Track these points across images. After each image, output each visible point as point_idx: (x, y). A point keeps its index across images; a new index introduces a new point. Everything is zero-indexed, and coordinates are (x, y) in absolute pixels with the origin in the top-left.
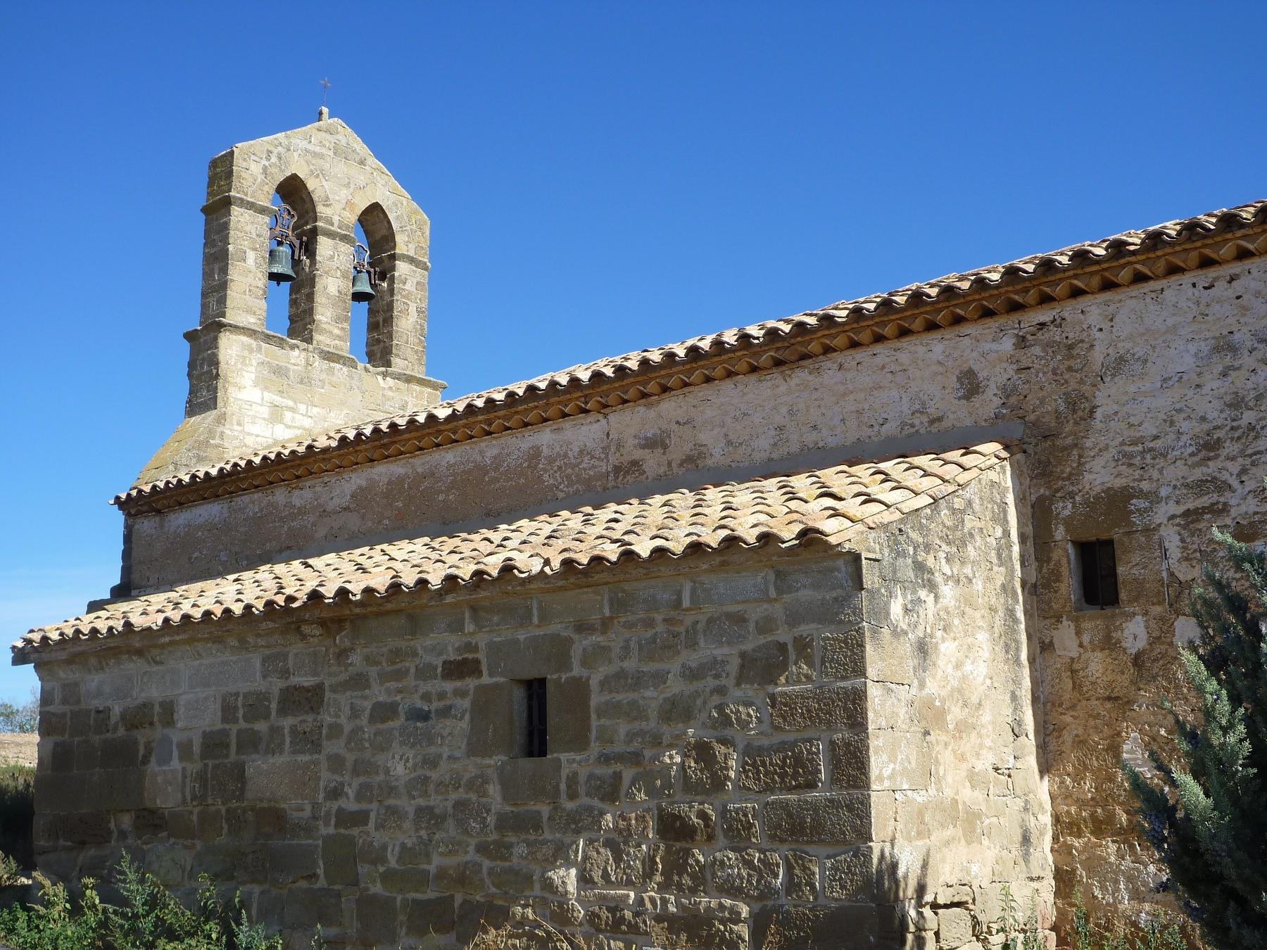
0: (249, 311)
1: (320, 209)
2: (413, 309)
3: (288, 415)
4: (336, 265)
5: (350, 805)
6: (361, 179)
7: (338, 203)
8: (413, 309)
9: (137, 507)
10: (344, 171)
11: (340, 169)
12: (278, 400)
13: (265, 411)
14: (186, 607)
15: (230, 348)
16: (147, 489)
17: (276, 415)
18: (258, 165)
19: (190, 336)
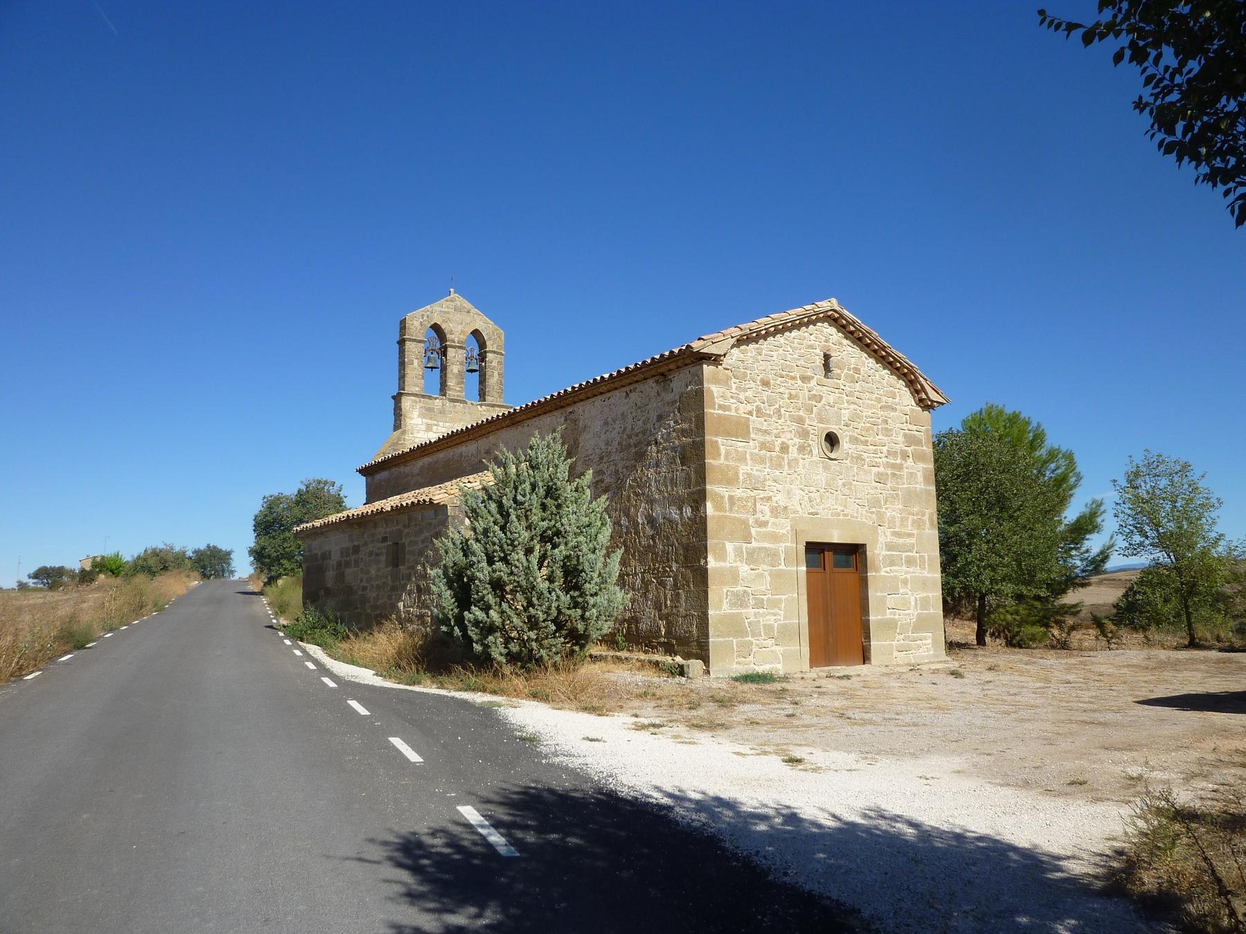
0: (416, 385)
1: (448, 336)
2: (496, 373)
3: (435, 428)
4: (456, 359)
5: (364, 584)
6: (468, 320)
7: (457, 330)
8: (496, 373)
9: (364, 471)
10: (459, 316)
11: (458, 317)
12: (430, 422)
13: (424, 427)
14: (424, 497)
15: (406, 403)
16: (632, 366)
17: (429, 428)
18: (418, 323)
19: (393, 397)
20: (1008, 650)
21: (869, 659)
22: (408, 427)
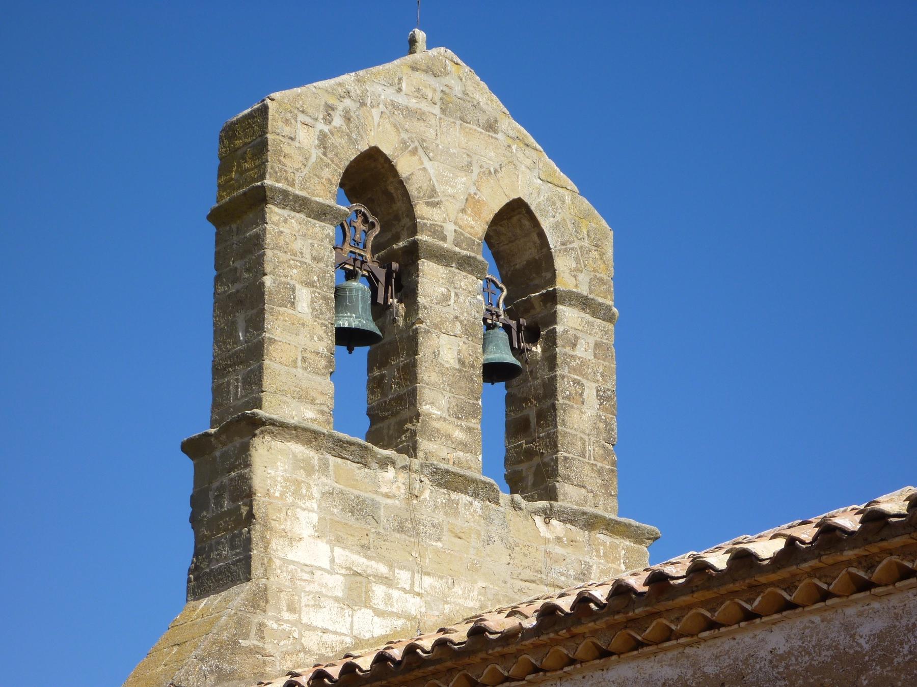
0: (304, 397)
1: (421, 210)
4: (452, 311)
6: (490, 156)
8: (590, 393)
12: (360, 562)
13: (336, 584)
15: (273, 466)
17: (357, 591)
18: (312, 131)
19: (195, 448)
20: (257, 570)
21: (240, 569)
22: (278, 578)
